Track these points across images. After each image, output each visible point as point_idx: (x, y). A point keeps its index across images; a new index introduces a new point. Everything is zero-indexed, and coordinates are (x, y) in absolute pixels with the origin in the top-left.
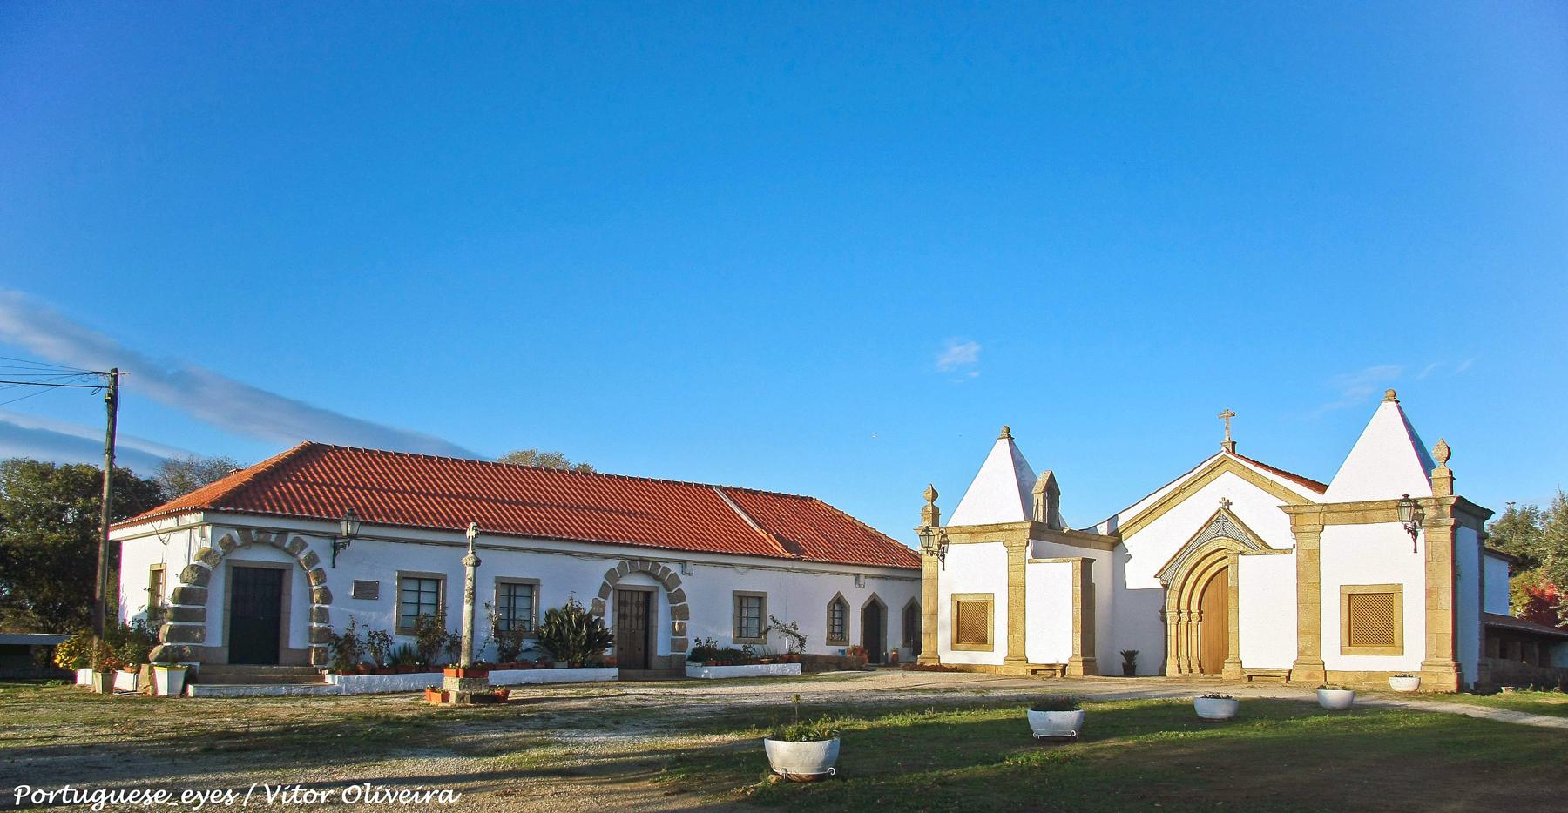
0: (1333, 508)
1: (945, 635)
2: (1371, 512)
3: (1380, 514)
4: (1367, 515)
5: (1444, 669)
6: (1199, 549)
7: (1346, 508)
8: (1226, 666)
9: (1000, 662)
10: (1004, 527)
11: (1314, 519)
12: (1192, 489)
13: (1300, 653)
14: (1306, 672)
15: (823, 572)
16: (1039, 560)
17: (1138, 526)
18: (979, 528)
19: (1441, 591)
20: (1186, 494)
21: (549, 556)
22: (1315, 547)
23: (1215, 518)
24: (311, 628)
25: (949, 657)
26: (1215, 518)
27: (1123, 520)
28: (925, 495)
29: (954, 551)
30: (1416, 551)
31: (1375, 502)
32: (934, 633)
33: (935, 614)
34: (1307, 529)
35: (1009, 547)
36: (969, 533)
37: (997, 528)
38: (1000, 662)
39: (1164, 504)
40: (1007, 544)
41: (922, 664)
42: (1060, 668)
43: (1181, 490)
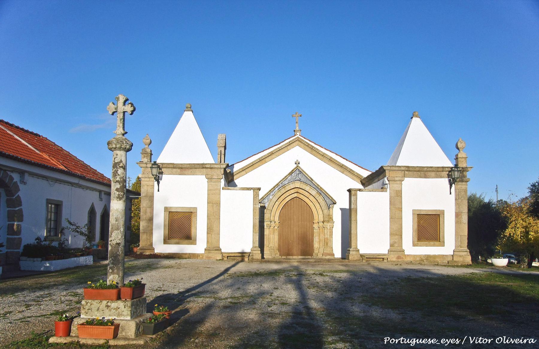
0: (411, 169)
1: (158, 235)
2: (429, 172)
3: (433, 174)
4: (426, 174)
5: (466, 253)
6: (284, 186)
7: (417, 169)
8: (351, 253)
9: (202, 251)
10: (207, 166)
11: (400, 174)
12: (277, 153)
13: (391, 245)
14: (396, 256)
15: (88, 188)
16: (230, 188)
17: (244, 172)
18: (188, 166)
19: (462, 214)
20: (273, 156)
21: (262, 153)
22: (400, 189)
23: (294, 170)
24: (117, 253)
25: (160, 248)
26: (294, 170)
27: (236, 168)
28: (144, 141)
29: (166, 178)
30: (451, 194)
31: (433, 167)
32: (150, 232)
33: (151, 220)
34: (396, 179)
35: (210, 179)
36: (179, 168)
37: (203, 166)
38: (202, 251)
39: (261, 161)
40: (209, 176)
41: (141, 254)
42: (248, 255)
43: (272, 154)
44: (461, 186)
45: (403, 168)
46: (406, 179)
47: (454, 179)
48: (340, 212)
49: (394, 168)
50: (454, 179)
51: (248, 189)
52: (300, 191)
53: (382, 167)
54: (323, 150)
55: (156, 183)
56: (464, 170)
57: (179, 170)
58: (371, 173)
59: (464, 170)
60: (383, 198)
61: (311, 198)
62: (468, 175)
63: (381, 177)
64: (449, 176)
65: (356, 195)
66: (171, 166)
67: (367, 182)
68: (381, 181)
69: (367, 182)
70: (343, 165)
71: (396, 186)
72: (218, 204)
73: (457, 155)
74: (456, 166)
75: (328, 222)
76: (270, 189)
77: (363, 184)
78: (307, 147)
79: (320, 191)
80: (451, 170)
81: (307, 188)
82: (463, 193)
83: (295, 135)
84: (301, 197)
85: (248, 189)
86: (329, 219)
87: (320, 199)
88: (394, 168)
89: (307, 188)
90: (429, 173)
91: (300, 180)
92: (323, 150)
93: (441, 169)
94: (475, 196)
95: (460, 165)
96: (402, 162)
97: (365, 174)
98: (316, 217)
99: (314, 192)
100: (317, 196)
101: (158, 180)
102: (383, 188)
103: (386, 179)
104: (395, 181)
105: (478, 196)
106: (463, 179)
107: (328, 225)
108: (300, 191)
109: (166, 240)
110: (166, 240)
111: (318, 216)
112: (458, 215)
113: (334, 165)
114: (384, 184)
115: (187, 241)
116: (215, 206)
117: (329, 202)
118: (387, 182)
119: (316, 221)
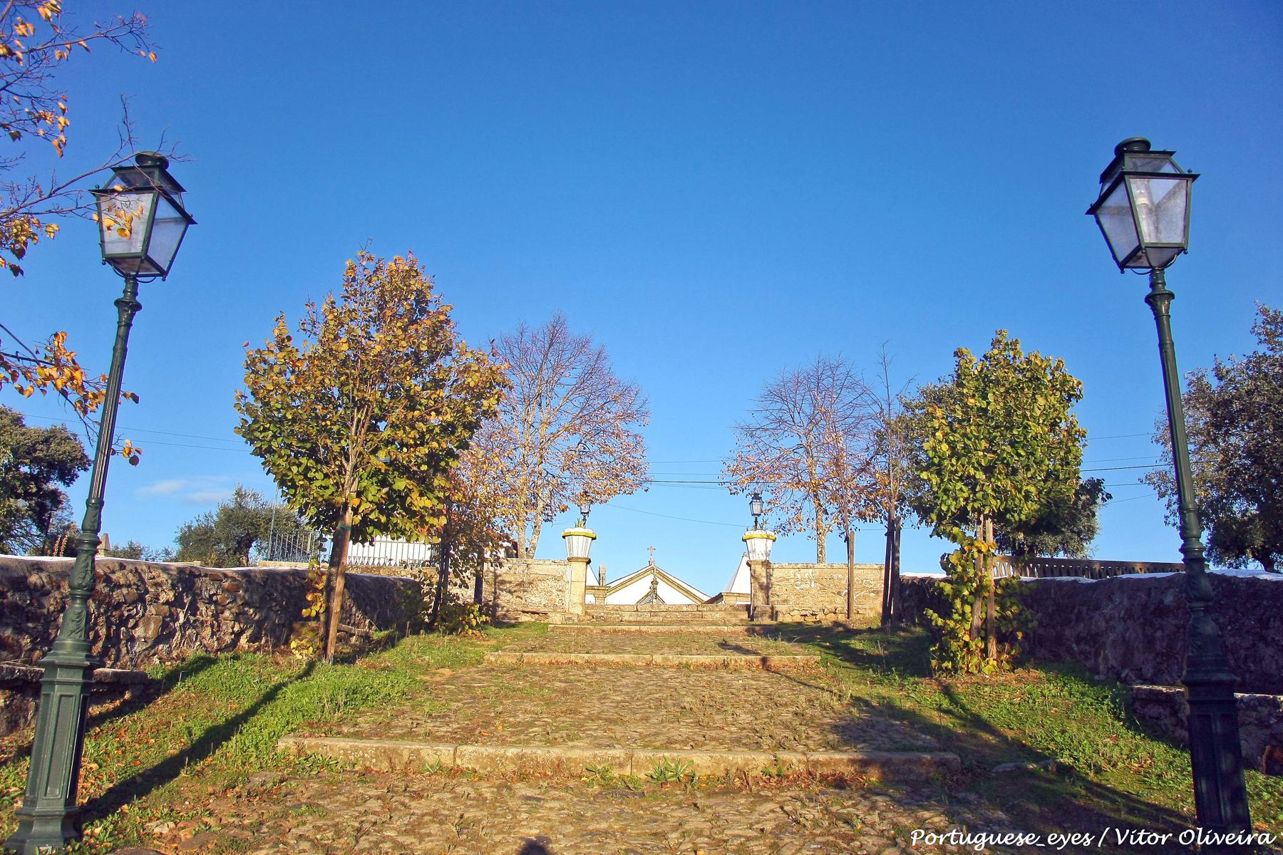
43: (622, 584)
97: (706, 599)
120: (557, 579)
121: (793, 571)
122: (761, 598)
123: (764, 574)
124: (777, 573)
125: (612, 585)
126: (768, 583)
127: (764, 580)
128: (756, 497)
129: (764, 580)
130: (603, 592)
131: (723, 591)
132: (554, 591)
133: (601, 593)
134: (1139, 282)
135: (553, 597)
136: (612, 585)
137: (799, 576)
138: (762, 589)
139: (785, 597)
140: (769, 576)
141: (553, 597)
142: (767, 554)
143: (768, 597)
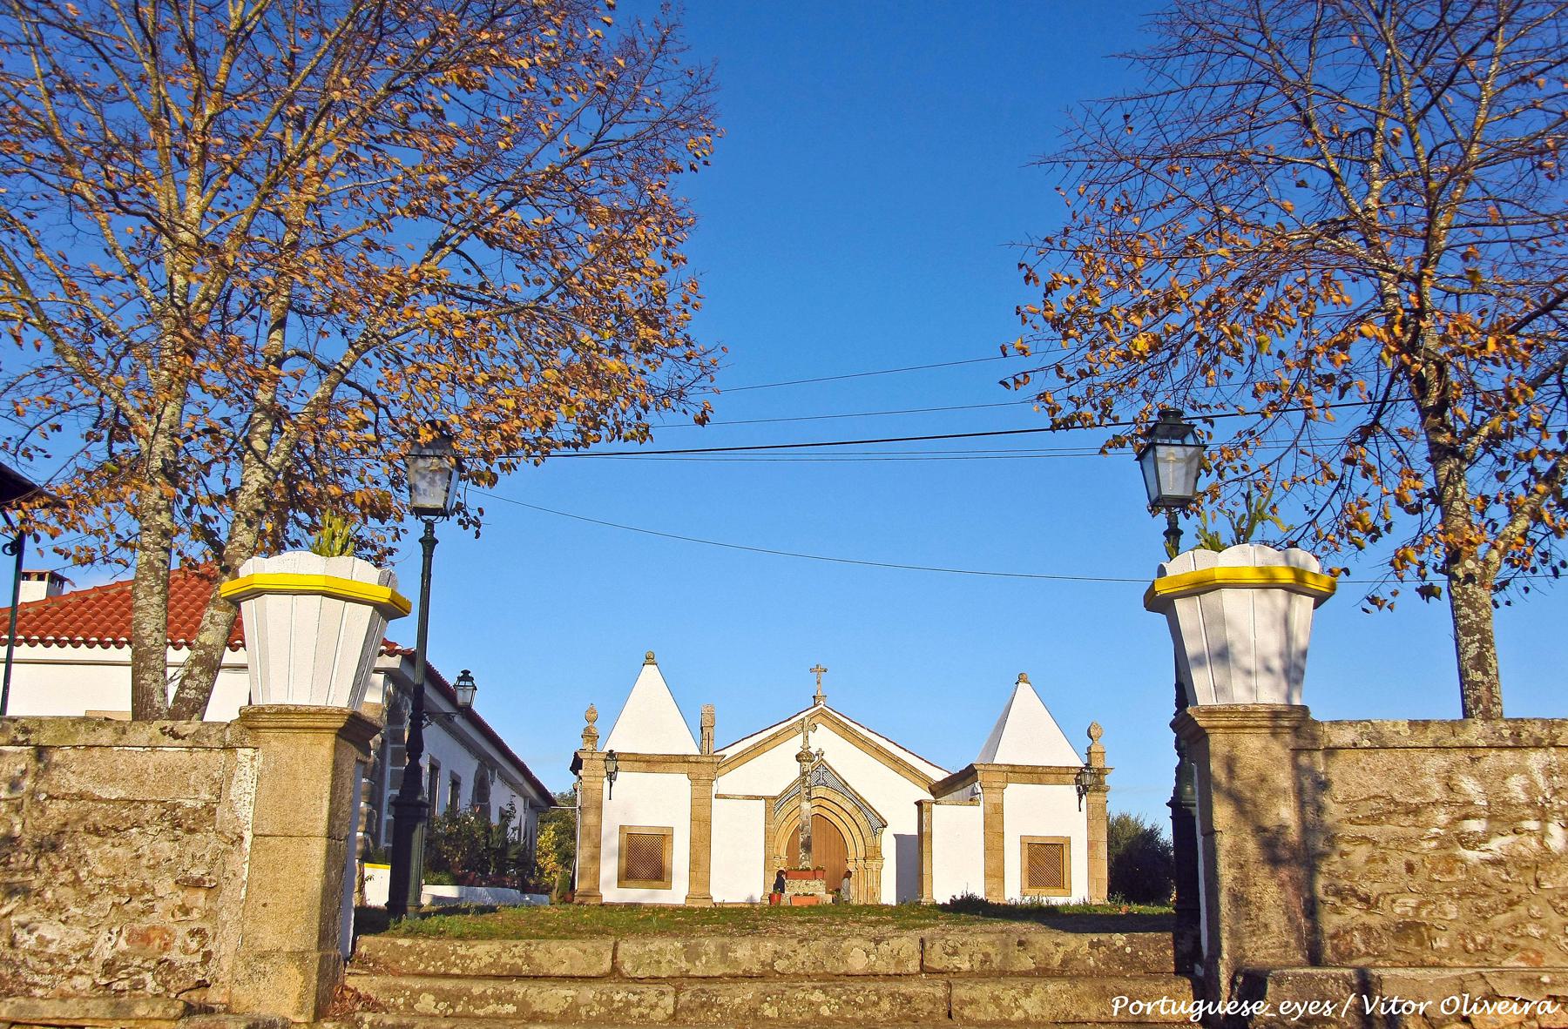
0: (1017, 769)
1: (609, 868)
3: (1052, 777)
7: (1029, 769)
10: (691, 759)
11: (1002, 777)
12: (785, 736)
25: (611, 893)
34: (995, 785)
37: (684, 759)
40: (693, 776)
43: (776, 736)
44: (1096, 798)
45: (1004, 768)
46: (1010, 786)
47: (1084, 787)
48: (893, 841)
49: (991, 768)
50: (1084, 787)
51: (757, 798)
52: (825, 803)
53: (971, 766)
54: (864, 732)
55: (607, 783)
56: (1102, 772)
57: (644, 765)
58: (947, 775)
59: (1102, 772)
60: (972, 816)
61: (844, 816)
62: (1108, 780)
63: (969, 781)
64: (1077, 781)
65: (930, 810)
66: (632, 758)
67: (941, 790)
68: (970, 788)
69: (941, 790)
70: (899, 759)
71: (994, 798)
72: (708, 823)
73: (1089, 748)
74: (1088, 766)
75: (874, 858)
76: (854, 784)
77: (933, 793)
78: (836, 727)
79: (861, 804)
80: (1081, 772)
81: (838, 799)
82: (1099, 810)
83: (815, 705)
84: (826, 813)
85: (757, 798)
86: (874, 853)
87: (860, 819)
88: (991, 768)
89: (838, 799)
90: (1047, 777)
91: (825, 784)
92: (864, 732)
93: (1065, 771)
94: (1127, 819)
95: (1093, 765)
96: (1004, 756)
97: (938, 776)
98: (851, 850)
99: (849, 806)
100: (854, 813)
101: (611, 777)
102: (972, 801)
103: (977, 784)
104: (992, 788)
105: (1133, 818)
106: (1099, 787)
107: (873, 864)
108: (825, 803)
109: (627, 876)
110: (627, 876)
111: (855, 848)
112: (1091, 845)
113: (883, 759)
114: (973, 793)
115: (656, 883)
116: (703, 825)
117: (876, 823)
118: (980, 790)
119: (851, 857)
120: (179, 823)
121: (1438, 762)
122: (1275, 919)
123: (1283, 778)
124: (1353, 775)
125: (730, 753)
126: (1306, 829)
127: (1285, 813)
128: (1171, 426)
129: (1285, 813)
130: (709, 769)
131: (974, 759)
132: (165, 886)
133: (703, 771)
134: (1162, 521)
135: (160, 917)
136: (730, 753)
137: (1470, 786)
138: (1274, 861)
139: (1405, 906)
140: (1311, 790)
141: (160, 917)
142: (1293, 671)
143: (1312, 909)
